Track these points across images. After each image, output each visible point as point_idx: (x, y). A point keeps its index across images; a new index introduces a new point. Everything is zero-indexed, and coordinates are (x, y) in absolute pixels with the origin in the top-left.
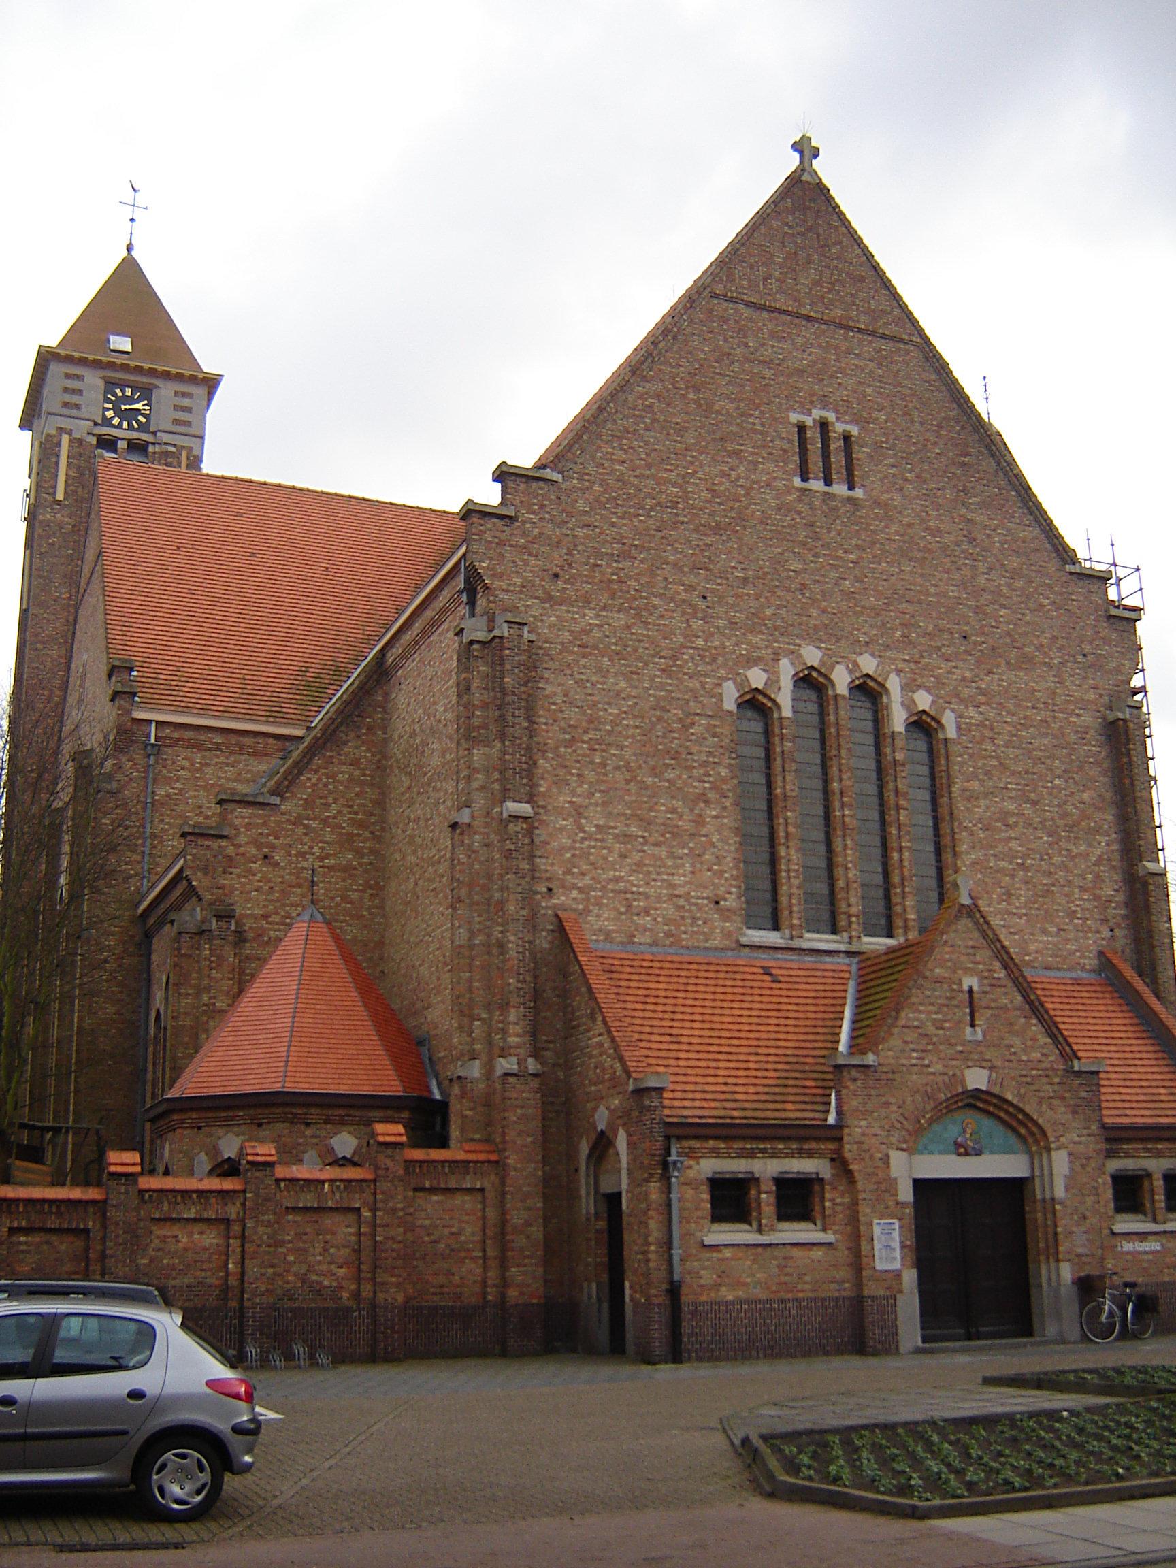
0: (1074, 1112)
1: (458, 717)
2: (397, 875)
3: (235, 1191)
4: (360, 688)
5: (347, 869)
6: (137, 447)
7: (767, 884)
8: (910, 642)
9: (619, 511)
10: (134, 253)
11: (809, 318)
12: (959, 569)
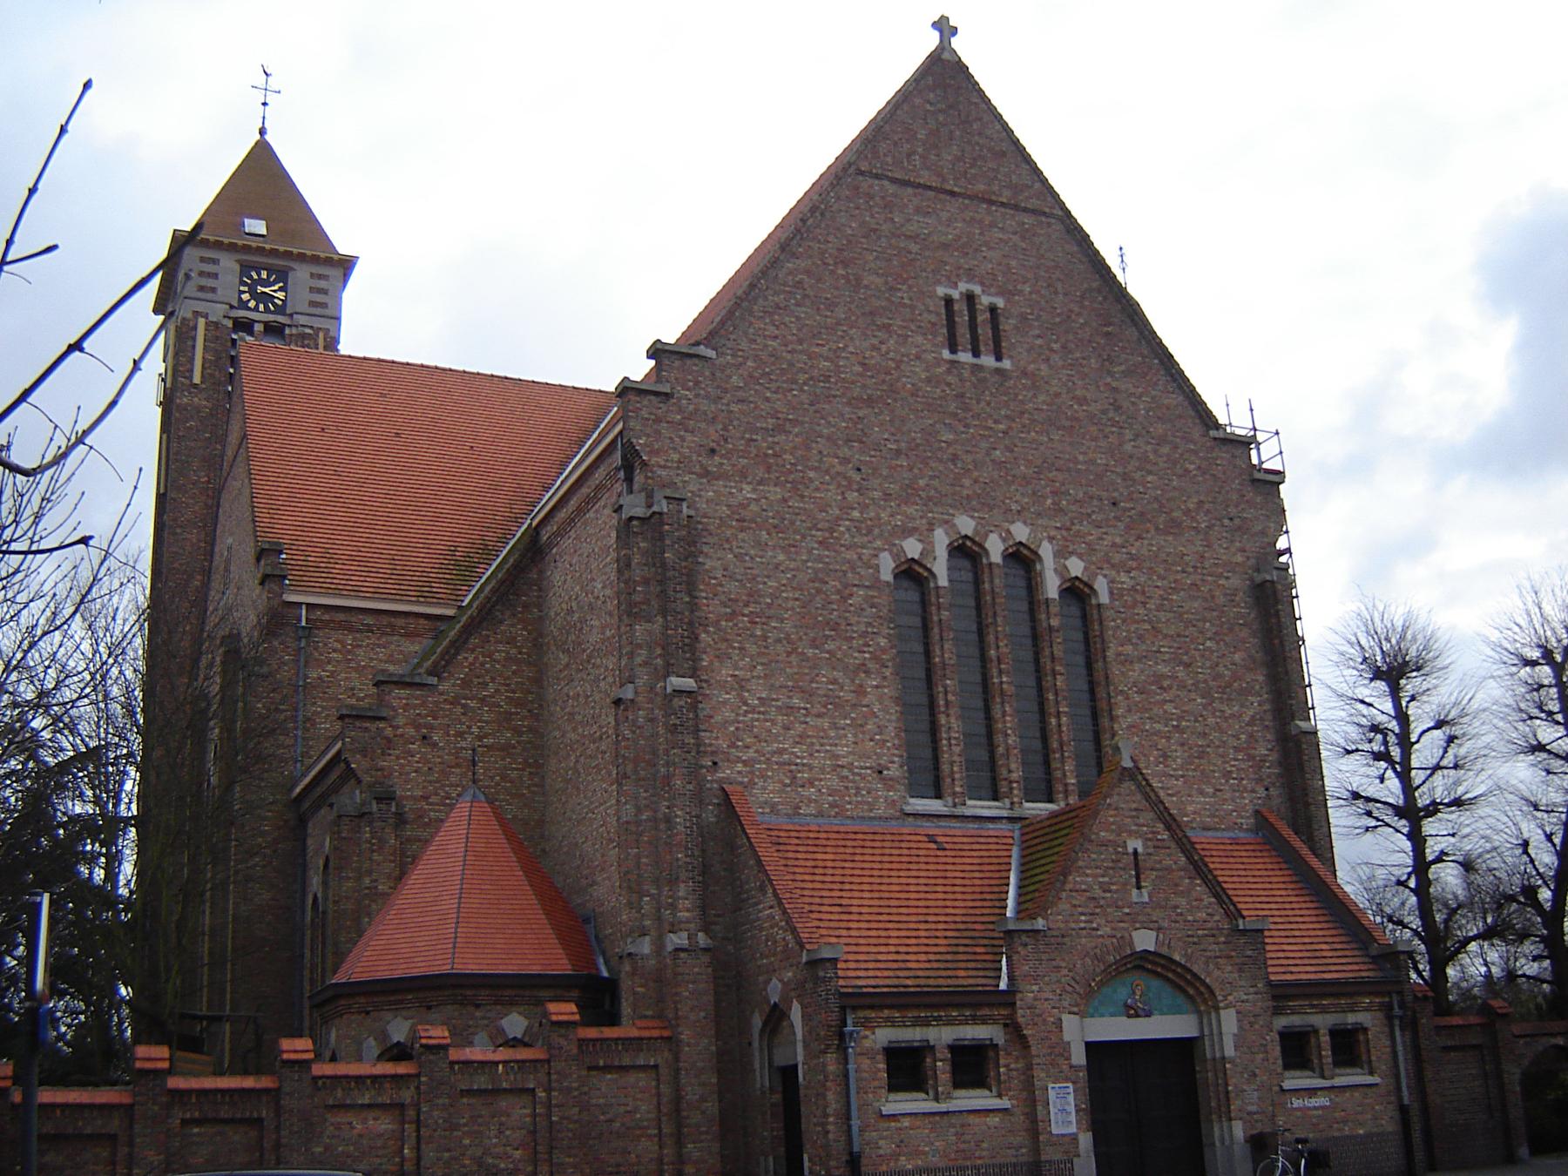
0: (1240, 971)
1: (618, 594)
2: (556, 753)
3: (409, 1076)
4: (515, 566)
5: (506, 749)
6: (274, 330)
7: (928, 753)
8: (1061, 510)
9: (773, 386)
10: (267, 137)
11: (952, 194)
12: (1106, 437)
